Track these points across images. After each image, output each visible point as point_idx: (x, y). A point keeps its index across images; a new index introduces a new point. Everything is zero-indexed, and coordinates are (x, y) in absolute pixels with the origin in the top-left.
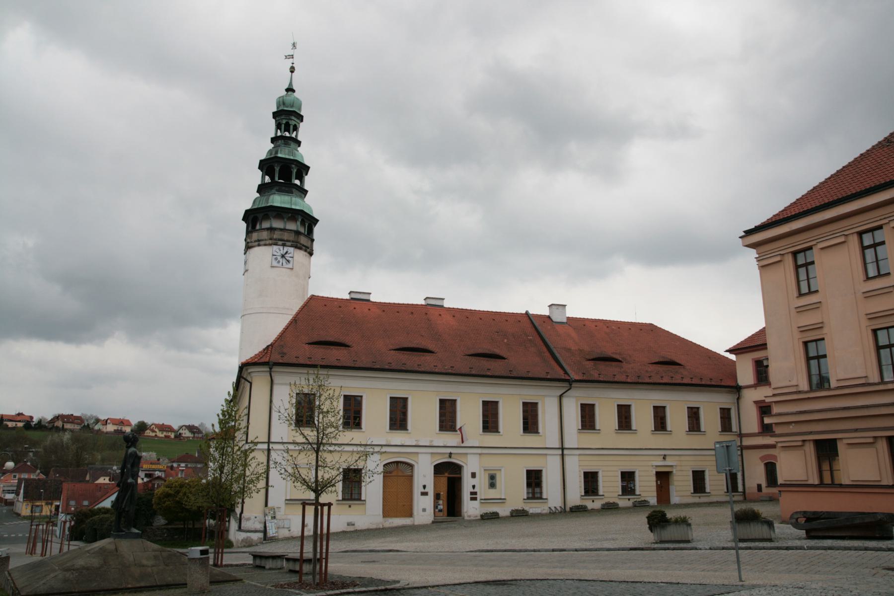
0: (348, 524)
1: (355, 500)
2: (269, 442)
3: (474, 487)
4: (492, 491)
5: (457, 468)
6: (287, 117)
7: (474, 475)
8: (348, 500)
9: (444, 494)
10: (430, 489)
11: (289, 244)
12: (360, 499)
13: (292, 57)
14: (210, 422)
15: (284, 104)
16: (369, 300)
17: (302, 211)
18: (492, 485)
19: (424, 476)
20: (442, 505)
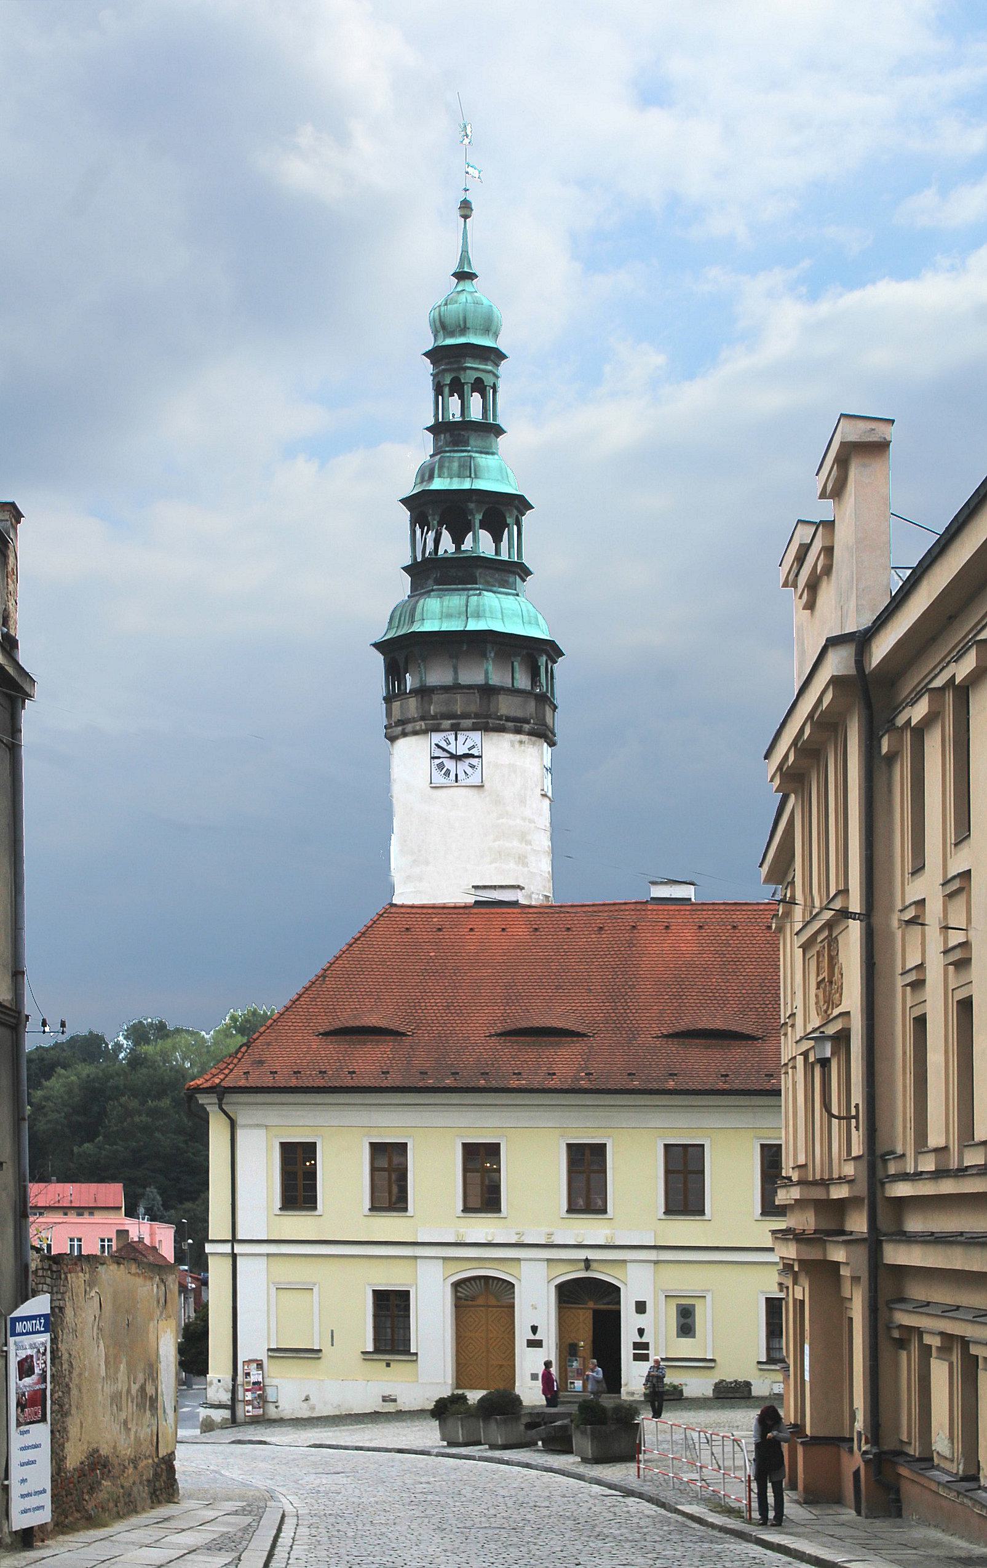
0: (385, 1399)
1: (399, 1352)
3: (641, 1332)
4: (685, 1341)
5: (612, 1292)
7: (641, 1307)
10: (549, 1334)
11: (468, 722)
12: (407, 1352)
15: (443, 326)
16: (515, 904)
18: (686, 1328)
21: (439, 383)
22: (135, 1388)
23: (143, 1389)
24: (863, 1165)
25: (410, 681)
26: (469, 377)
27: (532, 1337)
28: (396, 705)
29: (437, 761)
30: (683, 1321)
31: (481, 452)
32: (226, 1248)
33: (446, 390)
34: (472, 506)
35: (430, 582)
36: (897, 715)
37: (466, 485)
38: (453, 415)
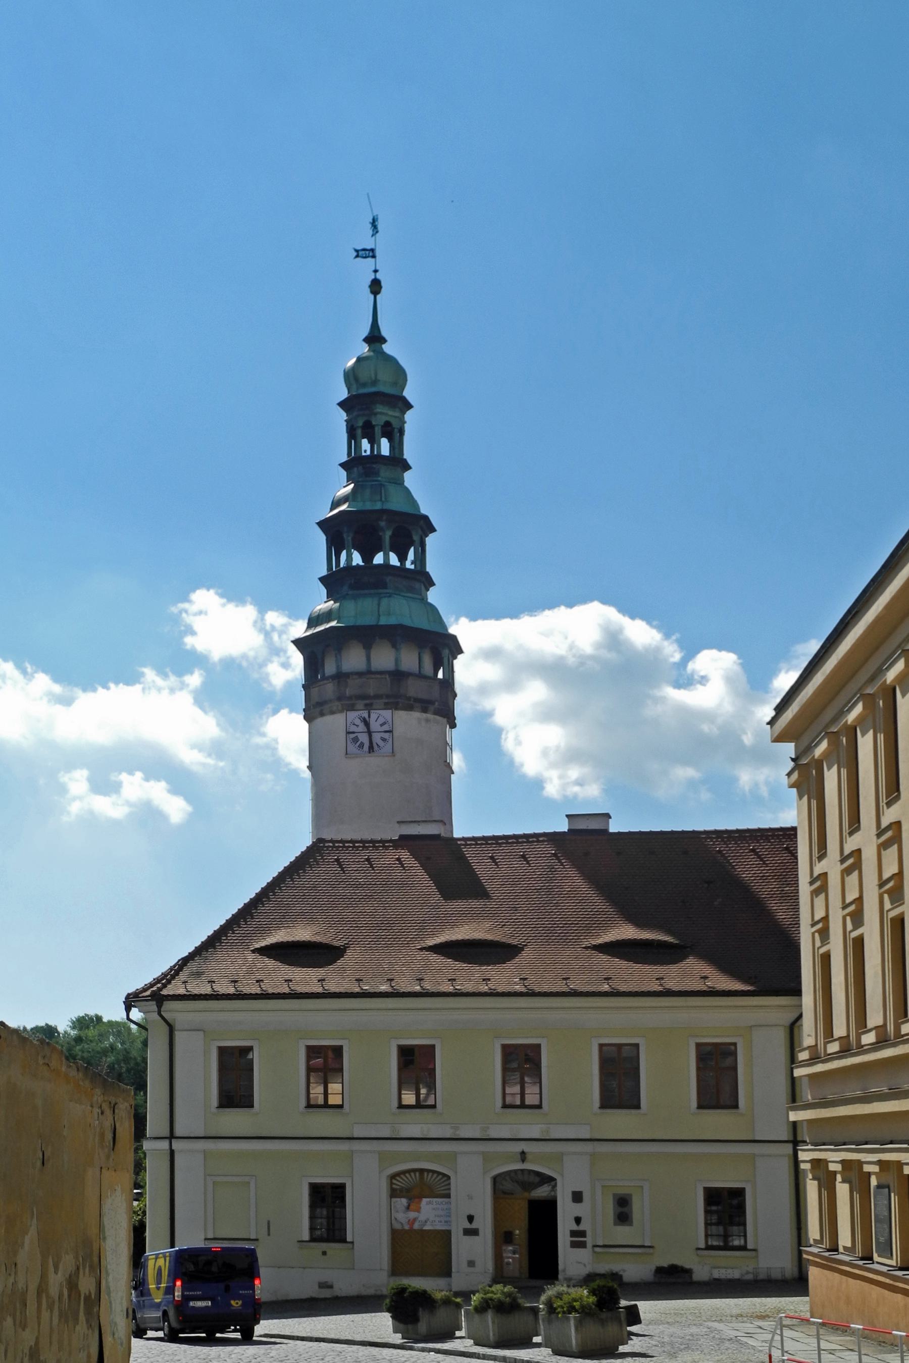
0: (324, 1285)
2: (172, 1136)
3: (578, 1220)
6: (374, 403)
7: (577, 1197)
9: (520, 1233)
10: (485, 1223)
12: (343, 1240)
13: (371, 253)
14: (845, 1035)
17: (401, 626)
20: (514, 1257)
21: (352, 426)
22: (56, 1281)
23: (72, 1284)
25: (330, 668)
26: (378, 421)
27: (468, 1226)
29: (352, 736)
30: (620, 1210)
32: (165, 1145)
33: (359, 432)
34: (382, 524)
35: (345, 588)
37: (378, 506)
38: (365, 451)
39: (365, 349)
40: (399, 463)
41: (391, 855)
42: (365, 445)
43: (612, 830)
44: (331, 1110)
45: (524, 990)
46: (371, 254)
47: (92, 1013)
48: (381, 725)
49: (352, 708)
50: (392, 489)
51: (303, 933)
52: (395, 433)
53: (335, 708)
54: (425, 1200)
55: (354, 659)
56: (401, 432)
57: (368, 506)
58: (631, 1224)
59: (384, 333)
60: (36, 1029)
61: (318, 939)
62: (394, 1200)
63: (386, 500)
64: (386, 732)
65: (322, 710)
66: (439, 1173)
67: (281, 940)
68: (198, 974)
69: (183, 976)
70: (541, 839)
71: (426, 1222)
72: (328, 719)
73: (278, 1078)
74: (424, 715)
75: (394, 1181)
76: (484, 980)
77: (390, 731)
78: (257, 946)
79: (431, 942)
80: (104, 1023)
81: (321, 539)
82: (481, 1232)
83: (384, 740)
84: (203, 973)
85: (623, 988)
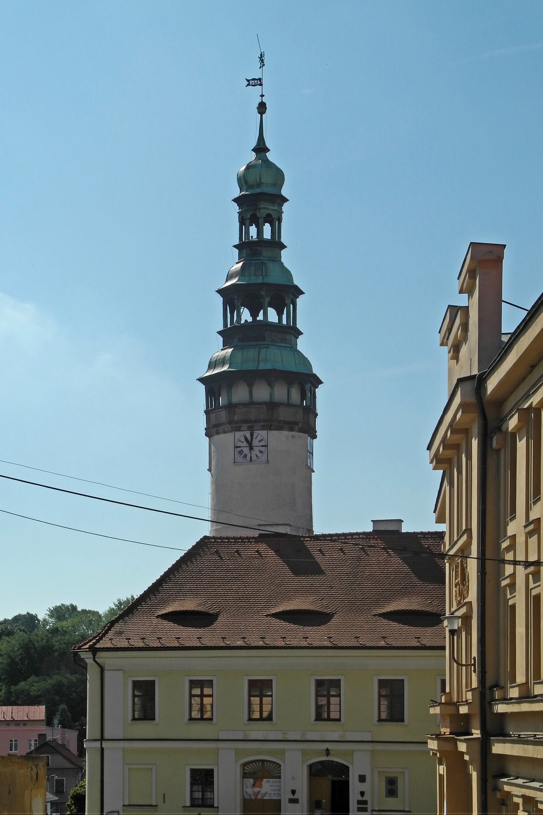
3: (362, 794)
4: (391, 800)
5: (345, 770)
6: (260, 197)
7: (362, 779)
8: (198, 806)
9: (326, 801)
10: (303, 795)
12: (212, 806)
13: (258, 82)
17: (275, 370)
19: (293, 778)
24: (477, 693)
26: (261, 214)
28: (213, 416)
29: (239, 449)
31: (269, 260)
32: (97, 744)
33: (247, 222)
34: (263, 293)
36: (503, 424)
37: (260, 281)
38: (252, 237)
39: (253, 155)
40: (277, 245)
41: (254, 547)
42: (253, 231)
43: (404, 531)
44: (205, 722)
45: (330, 645)
46: (259, 83)
47: (67, 603)
48: (259, 441)
49: (238, 429)
50: (271, 266)
51: (189, 604)
52: (275, 220)
53: (226, 429)
54: (265, 780)
55: (240, 394)
56: (280, 220)
57: (253, 280)
58: (397, 797)
59: (268, 145)
60: (17, 619)
61: (200, 609)
62: (245, 780)
63: (266, 275)
64: (262, 446)
65: (218, 430)
66: (274, 763)
67: (175, 610)
68: (120, 633)
69: (110, 634)
70: (354, 537)
71: (265, 794)
72: (222, 436)
73: (171, 701)
74: (291, 433)
75: (245, 768)
76: (304, 638)
77: (266, 446)
78: (160, 613)
79: (273, 611)
80: (79, 612)
81: (220, 300)
82: (300, 801)
83: (261, 452)
84: (123, 632)
85: (394, 644)
